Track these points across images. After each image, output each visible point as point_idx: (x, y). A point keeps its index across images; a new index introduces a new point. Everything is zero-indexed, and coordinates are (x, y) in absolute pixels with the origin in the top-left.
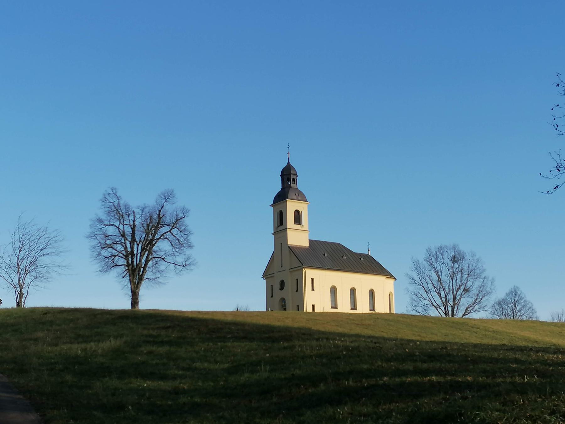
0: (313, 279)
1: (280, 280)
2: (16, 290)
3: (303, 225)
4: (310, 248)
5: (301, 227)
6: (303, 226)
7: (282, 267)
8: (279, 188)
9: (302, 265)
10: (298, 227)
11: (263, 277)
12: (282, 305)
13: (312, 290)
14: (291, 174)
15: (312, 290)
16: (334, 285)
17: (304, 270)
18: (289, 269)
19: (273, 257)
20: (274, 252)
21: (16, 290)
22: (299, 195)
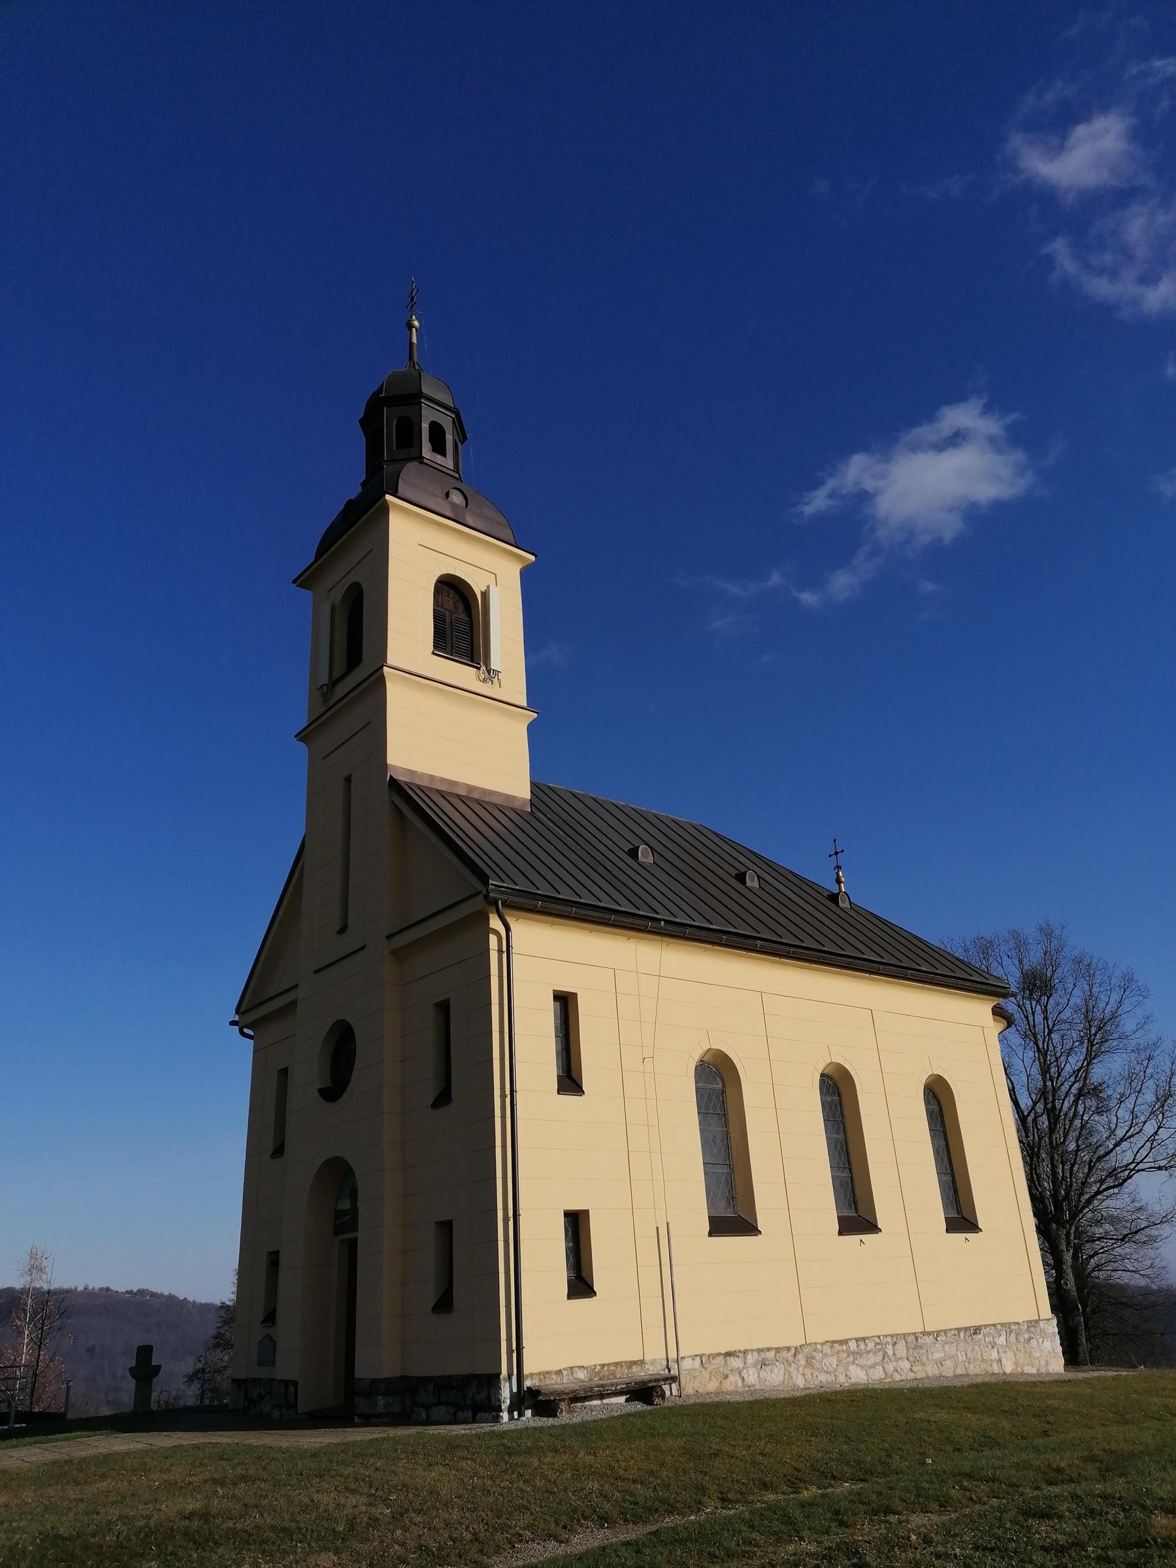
0: (565, 1002)
1: (331, 1021)
2: (1102, 1251)
3: (494, 665)
4: (535, 811)
5: (484, 681)
6: (497, 672)
7: (343, 930)
8: (355, 491)
9: (479, 886)
10: (462, 674)
11: (237, 1018)
12: (339, 1214)
13: (586, 1213)
14: (421, 395)
15: (586, 1213)
16: (716, 1046)
17: (495, 923)
18: (389, 937)
19: (299, 886)
20: (306, 839)
21: (1102, 1251)
22: (467, 506)
